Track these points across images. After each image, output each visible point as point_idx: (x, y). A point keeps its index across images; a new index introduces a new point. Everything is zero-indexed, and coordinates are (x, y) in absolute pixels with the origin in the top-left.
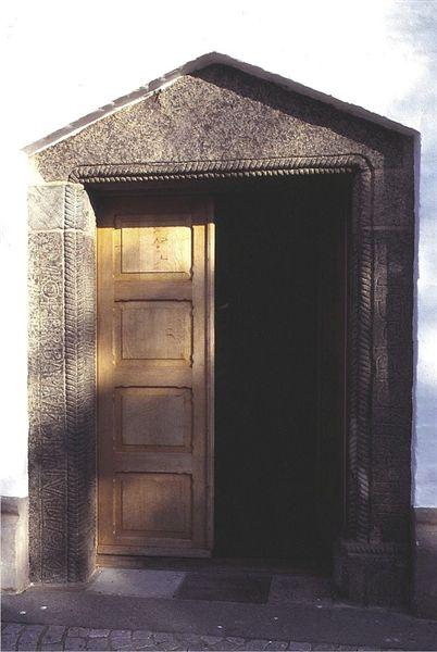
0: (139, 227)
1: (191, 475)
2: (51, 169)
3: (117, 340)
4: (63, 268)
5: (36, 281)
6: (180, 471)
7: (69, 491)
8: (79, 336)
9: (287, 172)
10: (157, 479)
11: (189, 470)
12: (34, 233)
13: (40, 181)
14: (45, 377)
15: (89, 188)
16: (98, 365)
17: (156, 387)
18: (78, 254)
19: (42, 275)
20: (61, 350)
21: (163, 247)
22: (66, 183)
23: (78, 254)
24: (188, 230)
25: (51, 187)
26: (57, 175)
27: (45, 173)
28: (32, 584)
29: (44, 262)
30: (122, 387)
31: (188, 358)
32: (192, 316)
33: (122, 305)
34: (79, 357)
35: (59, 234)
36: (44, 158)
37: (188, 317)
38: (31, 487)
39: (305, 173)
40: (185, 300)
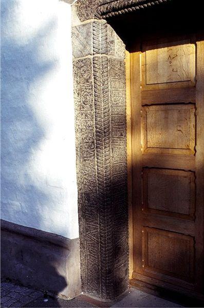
0: (157, 49)
1: (194, 238)
2: (83, 11)
3: (143, 128)
4: (93, 84)
5: (78, 94)
6: (187, 233)
7: (101, 239)
8: (105, 133)
9: (146, 5)
10: (170, 235)
11: (193, 234)
12: (76, 60)
13: (78, 22)
14: (85, 160)
15: (111, 21)
16: (135, 146)
17: (176, 169)
18: (103, 72)
19: (81, 90)
20: (93, 142)
21: (174, 62)
22: (93, 20)
23: (103, 72)
24: (193, 45)
25: (84, 25)
26: (87, 15)
27: (80, 15)
28: (82, 293)
29: (82, 80)
30: (147, 167)
31: (192, 149)
32: (196, 116)
33: (147, 109)
34: (105, 147)
35: (90, 59)
36: (80, 4)
37: (192, 116)
38: (80, 233)
39: (126, 12)
40: (190, 103)
